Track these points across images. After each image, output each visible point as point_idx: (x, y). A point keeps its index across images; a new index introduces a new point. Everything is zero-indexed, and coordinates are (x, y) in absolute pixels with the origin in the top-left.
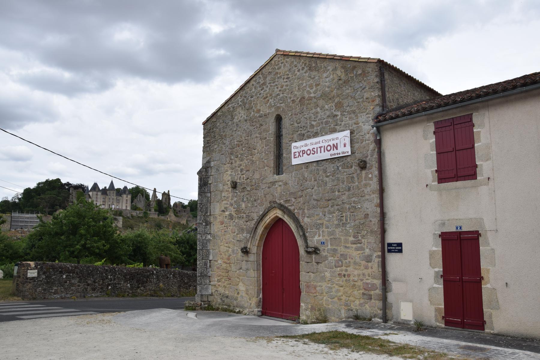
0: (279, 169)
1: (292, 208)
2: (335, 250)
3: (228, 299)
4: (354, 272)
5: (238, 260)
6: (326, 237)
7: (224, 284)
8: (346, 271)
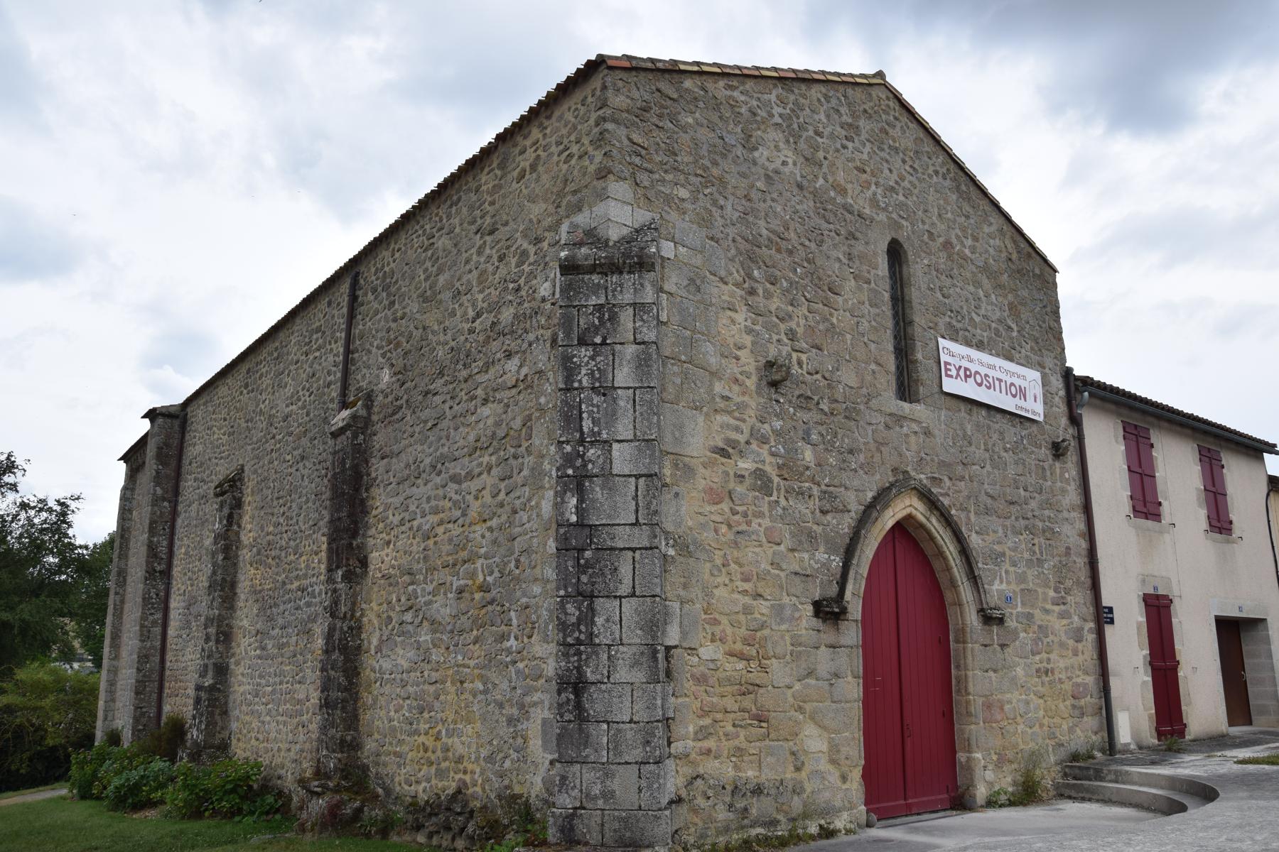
0: (906, 388)
1: (946, 501)
2: (1030, 617)
3: (762, 797)
4: (1060, 662)
5: (800, 645)
6: (1013, 586)
7: (736, 742)
8: (1049, 660)
